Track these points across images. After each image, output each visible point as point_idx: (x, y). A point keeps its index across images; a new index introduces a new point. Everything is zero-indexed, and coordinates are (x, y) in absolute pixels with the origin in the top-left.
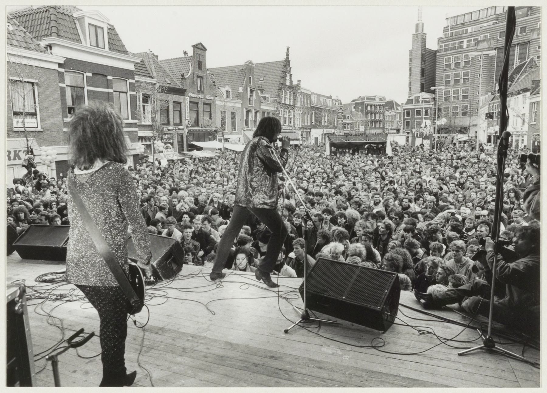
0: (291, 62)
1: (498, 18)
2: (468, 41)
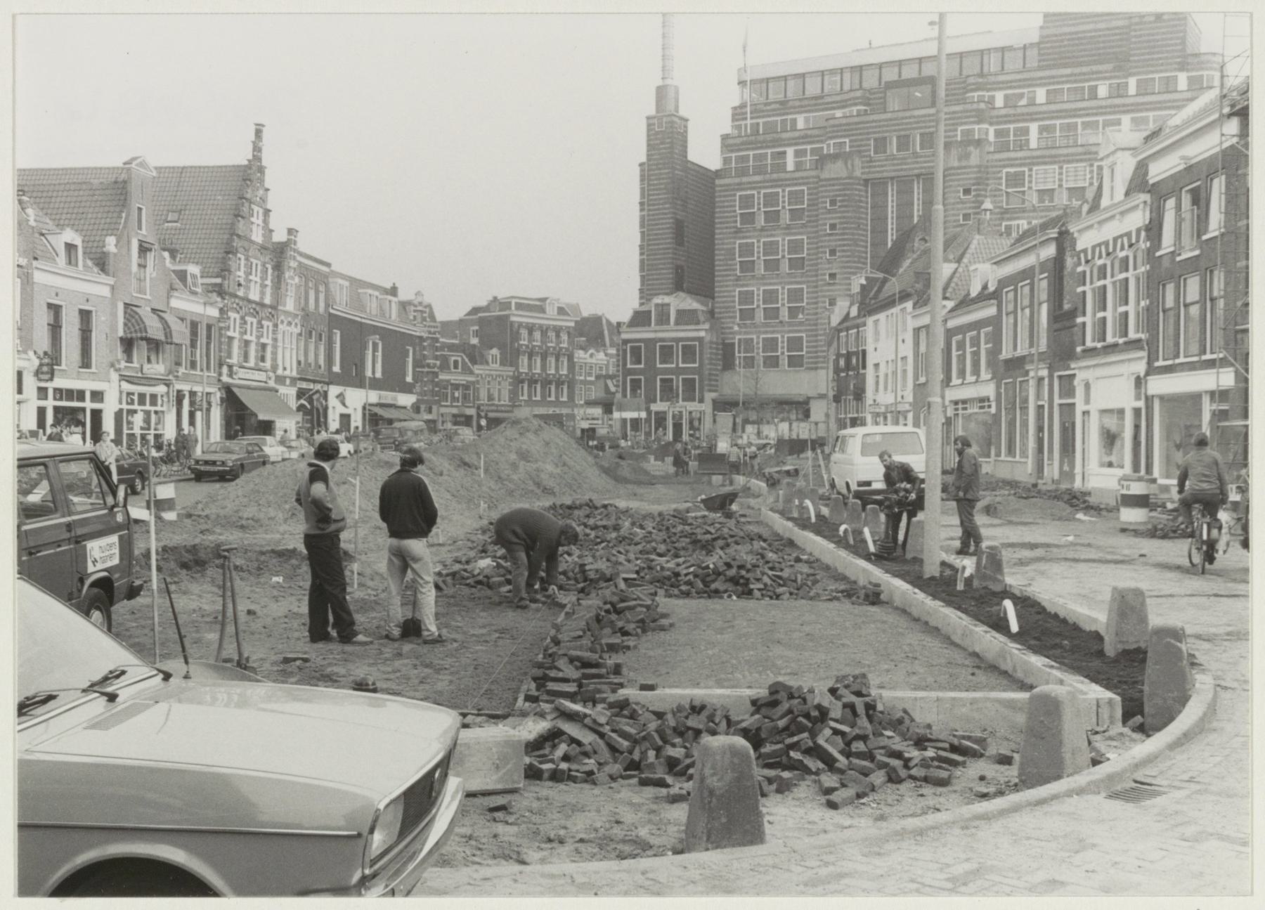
0: (267, 171)
1: (870, 99)
2: (798, 154)
